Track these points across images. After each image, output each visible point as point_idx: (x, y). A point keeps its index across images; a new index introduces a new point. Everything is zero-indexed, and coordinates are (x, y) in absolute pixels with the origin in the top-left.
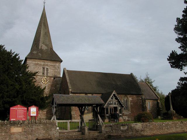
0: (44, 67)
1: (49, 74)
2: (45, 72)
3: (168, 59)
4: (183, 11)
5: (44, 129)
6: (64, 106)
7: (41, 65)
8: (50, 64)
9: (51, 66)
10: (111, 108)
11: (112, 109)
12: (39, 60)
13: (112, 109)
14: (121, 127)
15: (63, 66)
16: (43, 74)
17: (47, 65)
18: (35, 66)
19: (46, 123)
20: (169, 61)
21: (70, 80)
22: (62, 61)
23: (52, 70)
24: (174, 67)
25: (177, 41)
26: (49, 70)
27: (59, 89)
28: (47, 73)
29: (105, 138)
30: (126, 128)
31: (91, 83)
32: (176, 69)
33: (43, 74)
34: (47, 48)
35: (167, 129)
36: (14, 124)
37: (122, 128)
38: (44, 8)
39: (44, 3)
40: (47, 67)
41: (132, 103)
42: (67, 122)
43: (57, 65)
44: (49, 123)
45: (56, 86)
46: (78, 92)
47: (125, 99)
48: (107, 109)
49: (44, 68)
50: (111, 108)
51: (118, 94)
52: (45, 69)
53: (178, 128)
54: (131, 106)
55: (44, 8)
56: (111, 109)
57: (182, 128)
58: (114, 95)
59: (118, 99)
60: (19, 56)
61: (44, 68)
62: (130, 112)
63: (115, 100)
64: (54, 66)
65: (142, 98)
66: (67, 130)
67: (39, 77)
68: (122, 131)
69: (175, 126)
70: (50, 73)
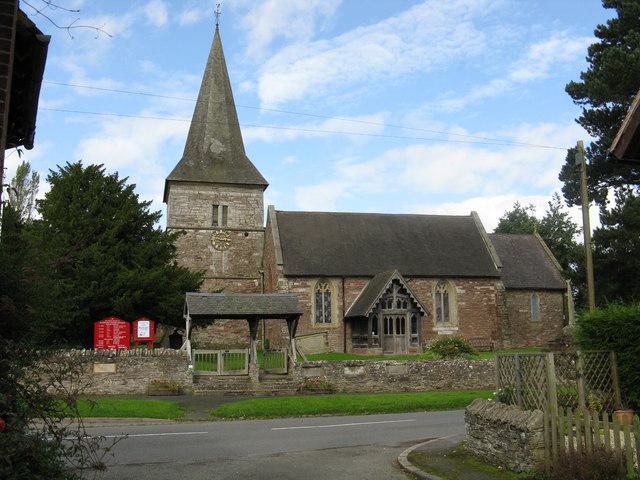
1: (229, 222)
2: (220, 216)
5: (162, 369)
7: (207, 198)
8: (231, 194)
9: (237, 198)
12: (202, 187)
14: (346, 369)
15: (275, 199)
16: (215, 222)
17: (226, 198)
19: (167, 355)
22: (264, 186)
26: (231, 213)
27: (258, 264)
28: (224, 222)
29: (354, 406)
30: (360, 371)
33: (215, 222)
36: (102, 359)
37: (347, 371)
38: (217, 30)
39: (217, 14)
40: (225, 203)
41: (462, 301)
42: (216, 355)
43: (255, 195)
44: (171, 356)
45: (250, 254)
47: (442, 291)
48: (375, 321)
49: (215, 207)
51: (404, 276)
52: (220, 209)
54: (460, 310)
55: (217, 30)
56: (386, 320)
58: (396, 281)
60: (34, 174)
61: (215, 207)
64: (245, 201)
65: (495, 288)
68: (347, 377)
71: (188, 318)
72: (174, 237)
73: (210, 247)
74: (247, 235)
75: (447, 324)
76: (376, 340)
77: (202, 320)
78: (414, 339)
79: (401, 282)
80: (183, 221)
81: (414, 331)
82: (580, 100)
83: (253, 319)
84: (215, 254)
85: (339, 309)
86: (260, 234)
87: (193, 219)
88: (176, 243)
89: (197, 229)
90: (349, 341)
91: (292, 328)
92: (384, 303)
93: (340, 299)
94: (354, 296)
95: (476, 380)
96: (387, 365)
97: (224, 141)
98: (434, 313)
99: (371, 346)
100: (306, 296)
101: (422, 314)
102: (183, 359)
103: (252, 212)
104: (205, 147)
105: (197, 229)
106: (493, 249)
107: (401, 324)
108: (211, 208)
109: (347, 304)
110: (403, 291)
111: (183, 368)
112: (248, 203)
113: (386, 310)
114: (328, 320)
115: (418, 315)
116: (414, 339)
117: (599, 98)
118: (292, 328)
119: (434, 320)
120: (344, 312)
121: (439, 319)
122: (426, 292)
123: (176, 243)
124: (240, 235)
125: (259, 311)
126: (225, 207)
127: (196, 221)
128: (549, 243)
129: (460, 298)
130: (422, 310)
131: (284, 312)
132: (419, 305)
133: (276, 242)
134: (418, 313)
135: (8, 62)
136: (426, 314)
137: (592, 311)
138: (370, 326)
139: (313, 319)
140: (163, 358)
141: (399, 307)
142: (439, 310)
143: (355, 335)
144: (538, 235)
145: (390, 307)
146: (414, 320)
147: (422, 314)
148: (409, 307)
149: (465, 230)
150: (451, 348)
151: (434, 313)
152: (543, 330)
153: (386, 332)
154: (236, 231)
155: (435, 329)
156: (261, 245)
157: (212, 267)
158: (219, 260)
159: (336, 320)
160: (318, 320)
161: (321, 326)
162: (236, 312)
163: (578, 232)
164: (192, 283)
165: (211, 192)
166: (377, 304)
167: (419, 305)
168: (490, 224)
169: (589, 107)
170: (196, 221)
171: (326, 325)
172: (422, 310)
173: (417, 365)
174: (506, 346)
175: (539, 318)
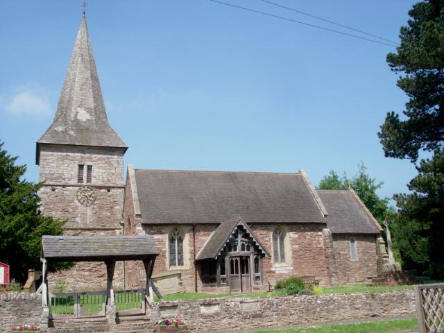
0: (82, 163)
3: (379, 134)
4: (412, 13)
6: (66, 261)
10: (234, 259)
11: (236, 261)
13: (237, 261)
14: (202, 308)
16: (80, 180)
18: (61, 162)
20: (380, 140)
21: (139, 193)
23: (103, 171)
24: (393, 155)
25: (114, 132)
27: (119, 216)
28: (89, 180)
30: (215, 309)
31: (191, 198)
32: (395, 159)
33: (80, 180)
34: (90, 118)
35: (328, 311)
37: (203, 310)
40: (90, 164)
46: (157, 222)
49: (81, 167)
50: (234, 259)
51: (248, 224)
52: (85, 168)
53: (358, 309)
54: (294, 252)
56: (232, 262)
57: (370, 310)
59: (251, 236)
62: (292, 268)
63: (244, 239)
65: (324, 233)
66: (73, 314)
67: (71, 188)
69: (352, 304)
70: (98, 177)
71: (44, 261)
72: (38, 187)
73: (76, 201)
74: (109, 191)
75: (284, 264)
76: (224, 279)
77: (57, 264)
78: (257, 278)
79: (245, 228)
80: (52, 179)
81: (257, 271)
82: (398, 68)
83: (110, 261)
84: (81, 208)
85: (191, 253)
86: (121, 191)
87: (61, 177)
88: (39, 193)
89: (64, 186)
90: (199, 282)
91: (149, 269)
92: (230, 246)
93: (195, 246)
94: (203, 242)
95: (324, 313)
96: (241, 302)
97: (89, 110)
98: (272, 254)
99: (219, 286)
100: (161, 241)
101: (263, 255)
102: (36, 303)
103: (113, 171)
104: (73, 116)
105: (64, 186)
106: (319, 200)
107: (244, 262)
108: (77, 168)
109: (196, 249)
110: (246, 236)
111: (37, 313)
112: (110, 164)
113: (232, 253)
114: (181, 263)
115: (259, 257)
116: (257, 278)
117: (410, 68)
118: (149, 269)
119: (272, 261)
120: (195, 256)
121: (276, 259)
122: (266, 239)
123: (39, 193)
124: (103, 191)
125: (116, 252)
126: (90, 168)
127: (64, 179)
128: (361, 196)
129: (293, 241)
130: (263, 252)
131: (141, 252)
132: (260, 248)
133: (135, 195)
134: (260, 254)
135: (164, 244)
136: (266, 256)
137: (238, 251)
138: (219, 270)
139: (167, 263)
140: (17, 302)
141: (243, 249)
142: (276, 252)
143: (205, 276)
144: (352, 191)
145: (235, 250)
146: (256, 261)
147: (263, 255)
148: (252, 249)
149: (294, 187)
150: (295, 286)
151: (272, 254)
152: (360, 268)
153: (232, 272)
154: (100, 188)
155: (273, 269)
156: (122, 200)
157: (78, 219)
158: (85, 215)
159: (188, 263)
160: (172, 263)
161: (173, 268)
162: (92, 253)
163: (7, 296)
164: (54, 229)
165: (78, 155)
166: (225, 248)
167: (260, 248)
168: (314, 181)
169: (403, 74)
170: (64, 179)
171: (177, 268)
172: (263, 252)
173: (269, 301)
174: (334, 282)
175: (358, 258)
